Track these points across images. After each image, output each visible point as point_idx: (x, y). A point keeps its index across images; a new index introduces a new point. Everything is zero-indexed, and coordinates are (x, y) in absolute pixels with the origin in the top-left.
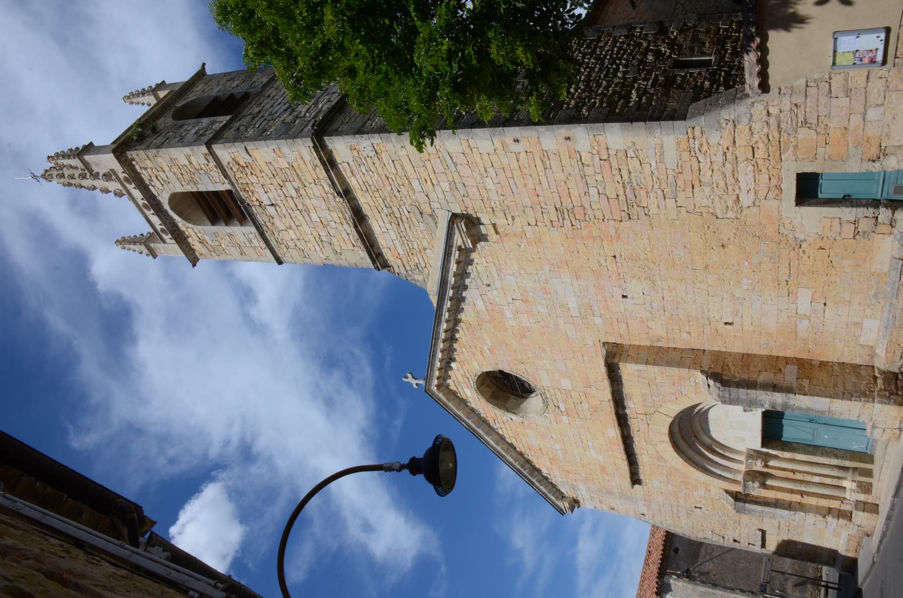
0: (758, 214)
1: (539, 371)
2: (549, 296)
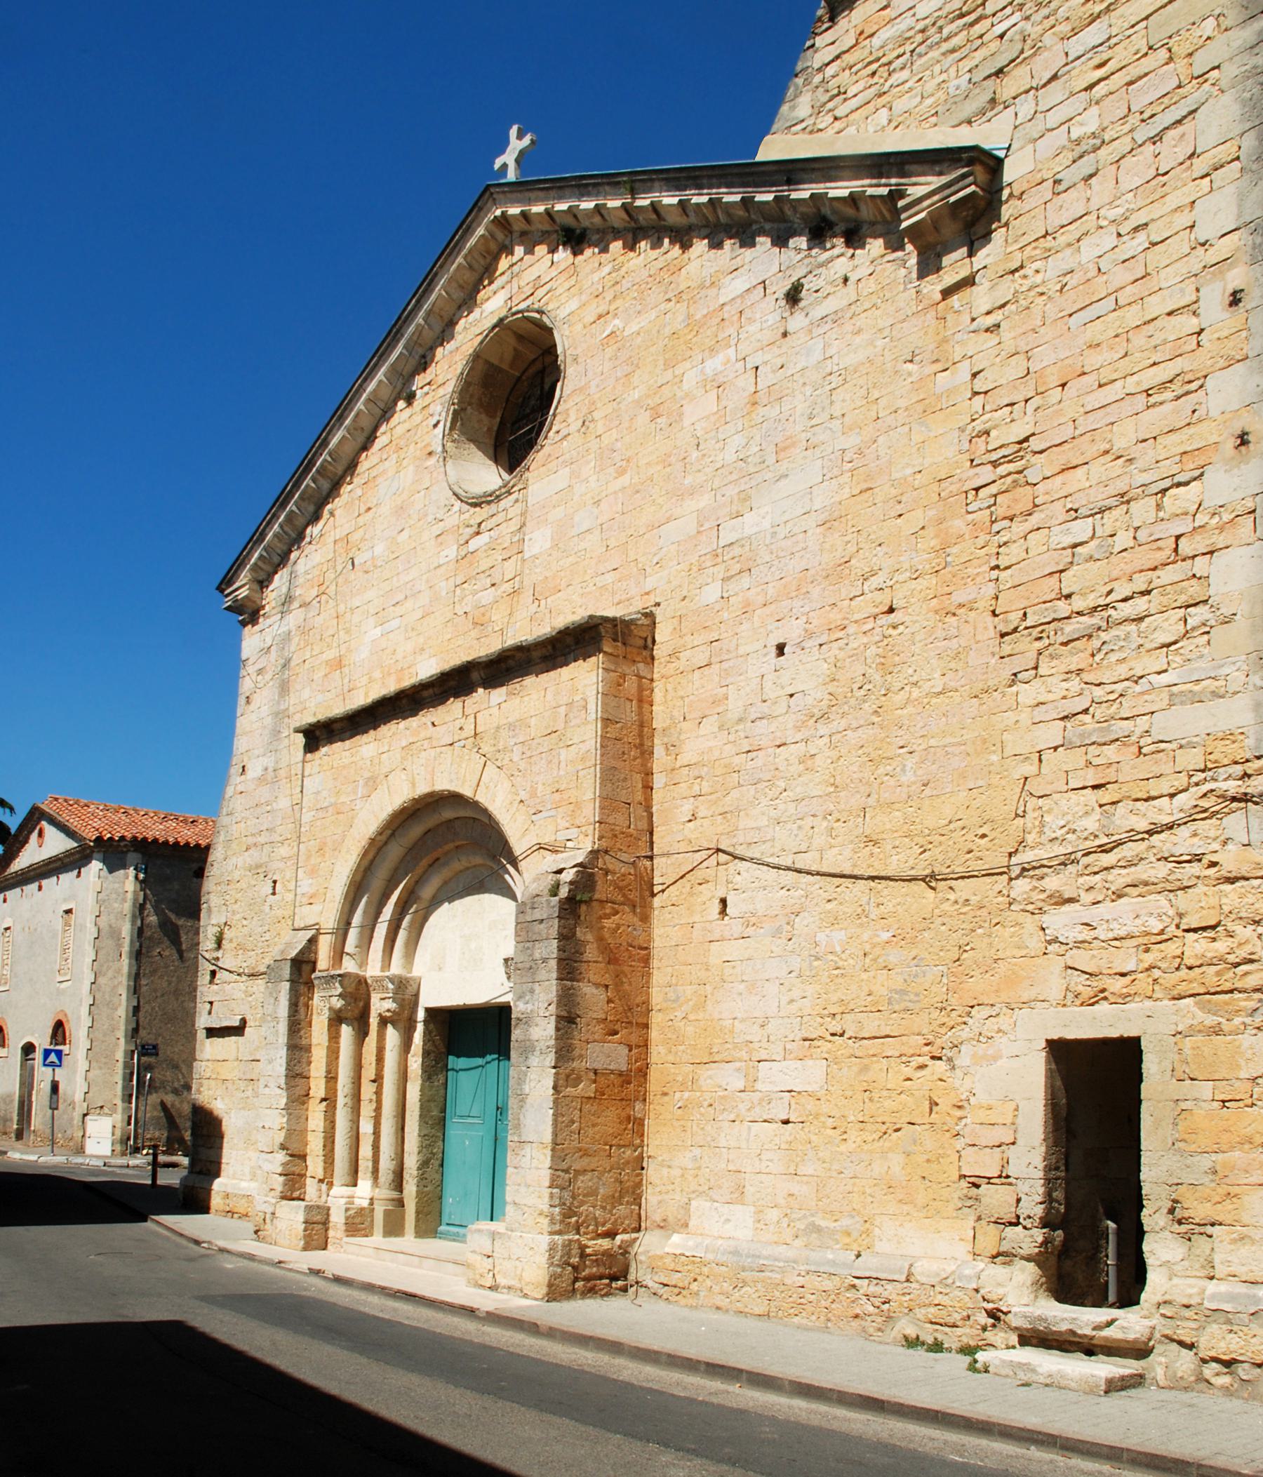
0: (1023, 953)
1: (567, 469)
2: (771, 459)
